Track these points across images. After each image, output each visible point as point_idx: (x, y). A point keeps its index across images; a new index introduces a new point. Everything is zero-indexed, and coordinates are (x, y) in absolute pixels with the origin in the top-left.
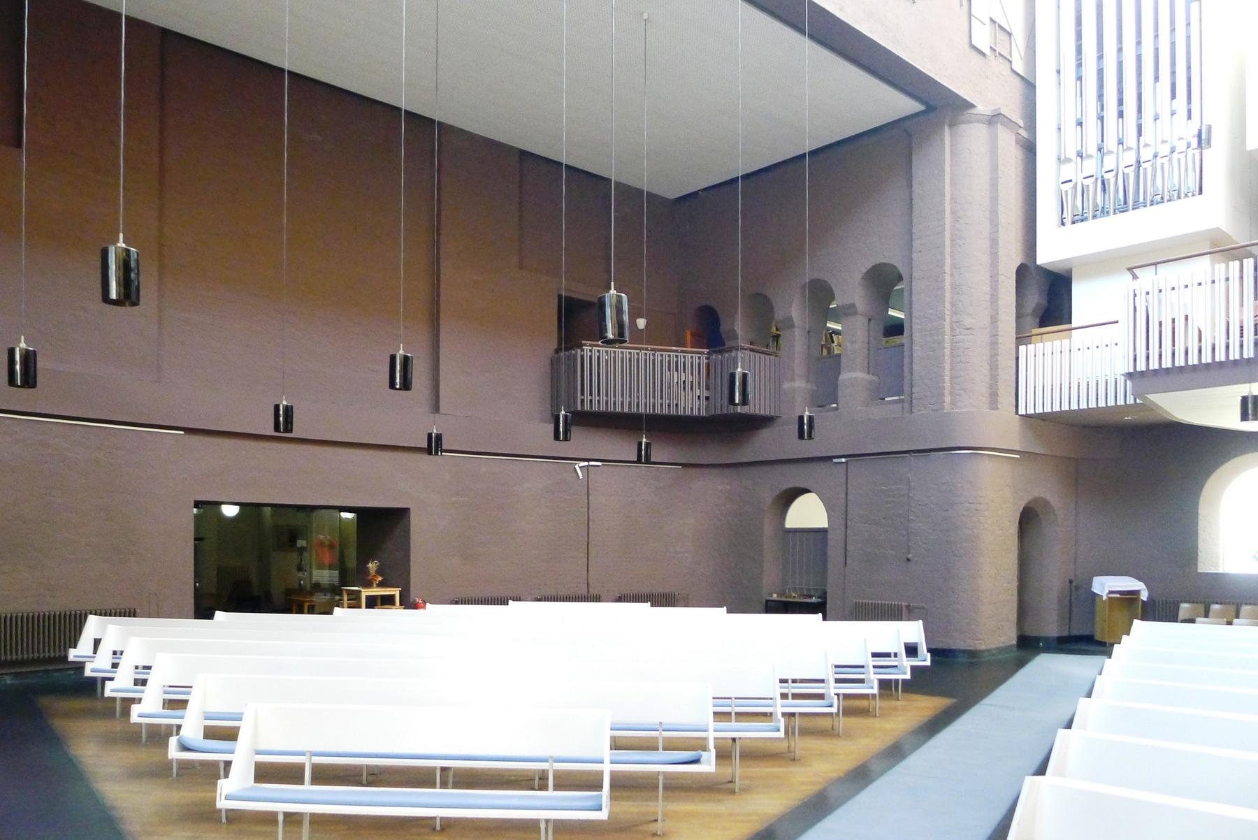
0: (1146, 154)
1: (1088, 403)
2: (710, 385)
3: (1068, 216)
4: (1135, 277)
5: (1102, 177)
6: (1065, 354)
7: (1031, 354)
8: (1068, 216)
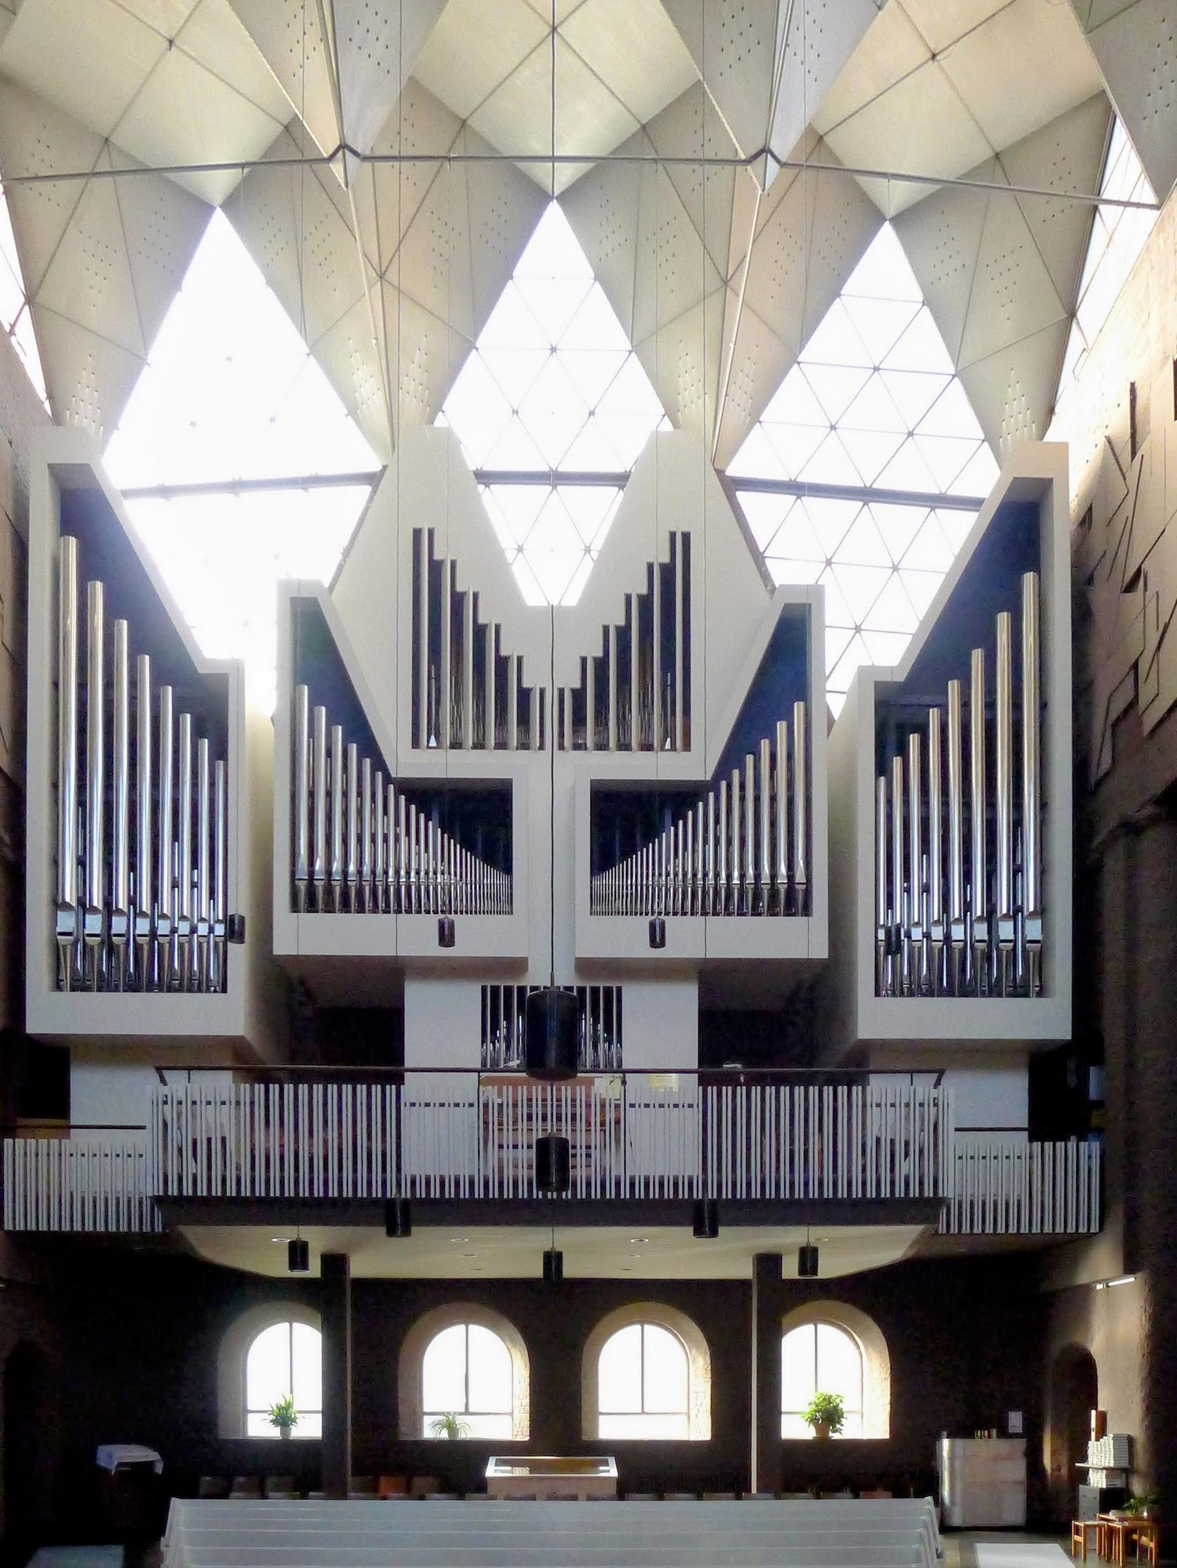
0: (163, 927)
1: (72, 1221)
2: (592, 1051)
3: (66, 976)
4: (163, 1081)
5: (84, 939)
6: (54, 1160)
7: (20, 1152)
8: (66, 976)
